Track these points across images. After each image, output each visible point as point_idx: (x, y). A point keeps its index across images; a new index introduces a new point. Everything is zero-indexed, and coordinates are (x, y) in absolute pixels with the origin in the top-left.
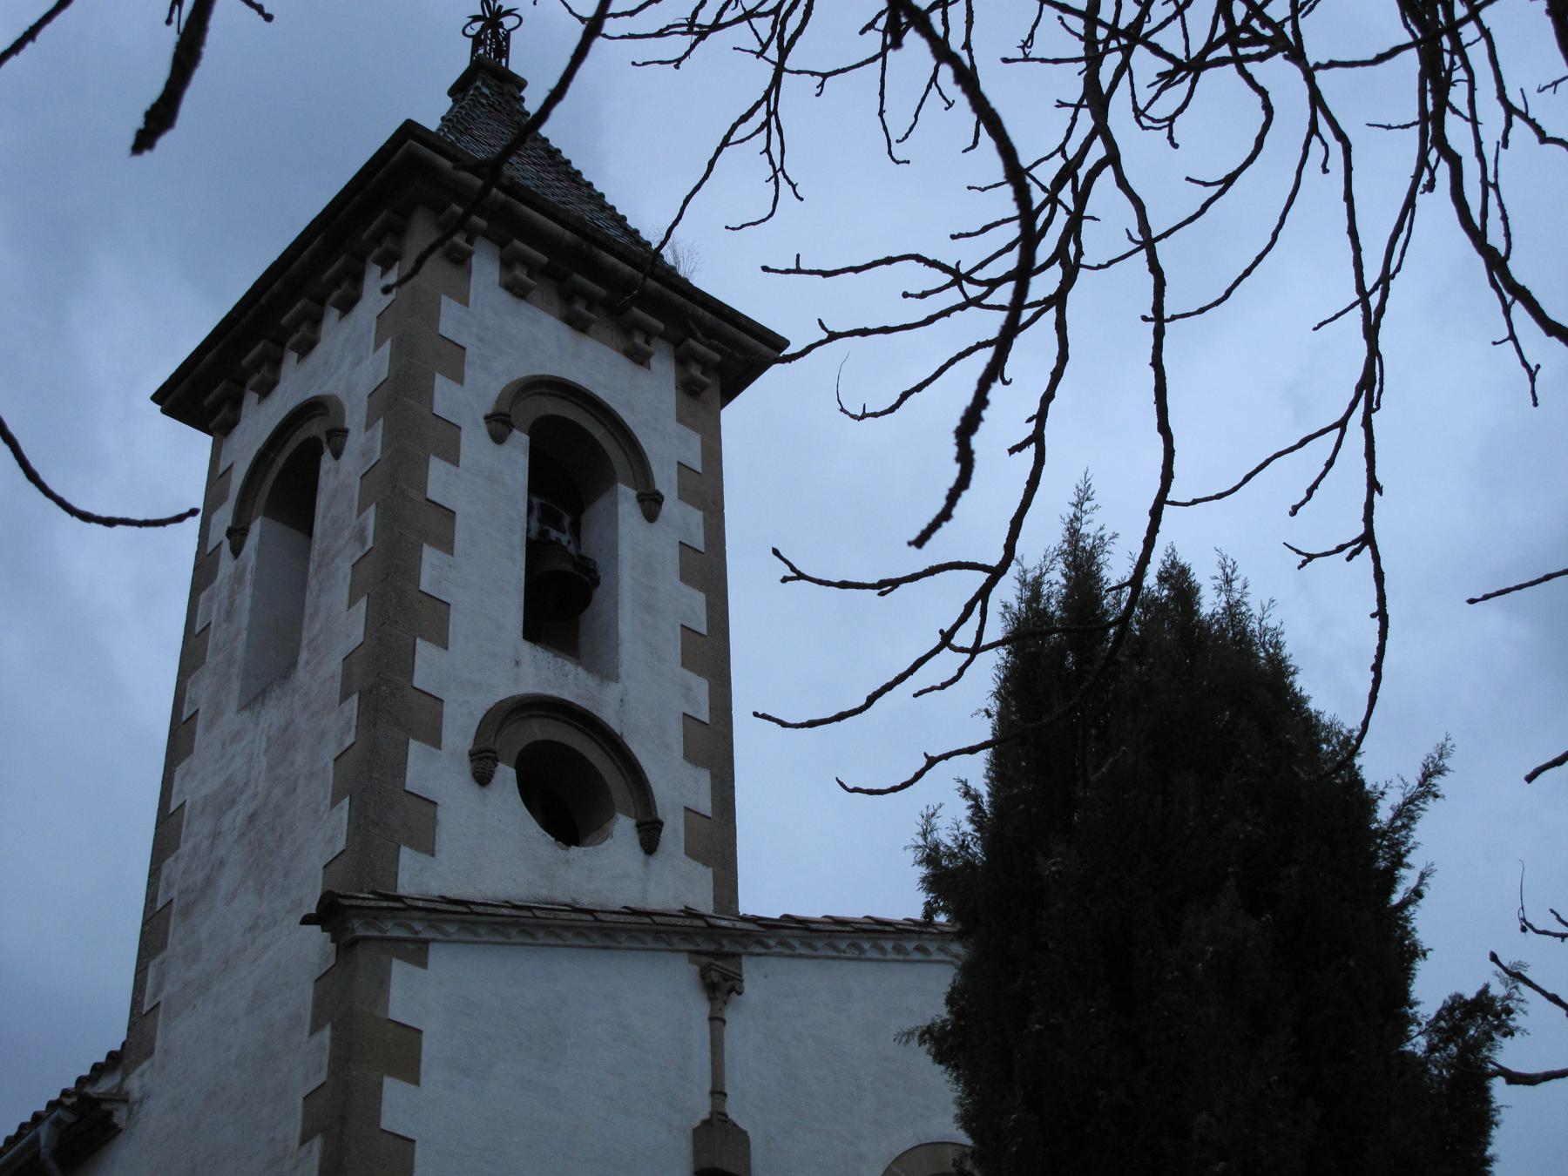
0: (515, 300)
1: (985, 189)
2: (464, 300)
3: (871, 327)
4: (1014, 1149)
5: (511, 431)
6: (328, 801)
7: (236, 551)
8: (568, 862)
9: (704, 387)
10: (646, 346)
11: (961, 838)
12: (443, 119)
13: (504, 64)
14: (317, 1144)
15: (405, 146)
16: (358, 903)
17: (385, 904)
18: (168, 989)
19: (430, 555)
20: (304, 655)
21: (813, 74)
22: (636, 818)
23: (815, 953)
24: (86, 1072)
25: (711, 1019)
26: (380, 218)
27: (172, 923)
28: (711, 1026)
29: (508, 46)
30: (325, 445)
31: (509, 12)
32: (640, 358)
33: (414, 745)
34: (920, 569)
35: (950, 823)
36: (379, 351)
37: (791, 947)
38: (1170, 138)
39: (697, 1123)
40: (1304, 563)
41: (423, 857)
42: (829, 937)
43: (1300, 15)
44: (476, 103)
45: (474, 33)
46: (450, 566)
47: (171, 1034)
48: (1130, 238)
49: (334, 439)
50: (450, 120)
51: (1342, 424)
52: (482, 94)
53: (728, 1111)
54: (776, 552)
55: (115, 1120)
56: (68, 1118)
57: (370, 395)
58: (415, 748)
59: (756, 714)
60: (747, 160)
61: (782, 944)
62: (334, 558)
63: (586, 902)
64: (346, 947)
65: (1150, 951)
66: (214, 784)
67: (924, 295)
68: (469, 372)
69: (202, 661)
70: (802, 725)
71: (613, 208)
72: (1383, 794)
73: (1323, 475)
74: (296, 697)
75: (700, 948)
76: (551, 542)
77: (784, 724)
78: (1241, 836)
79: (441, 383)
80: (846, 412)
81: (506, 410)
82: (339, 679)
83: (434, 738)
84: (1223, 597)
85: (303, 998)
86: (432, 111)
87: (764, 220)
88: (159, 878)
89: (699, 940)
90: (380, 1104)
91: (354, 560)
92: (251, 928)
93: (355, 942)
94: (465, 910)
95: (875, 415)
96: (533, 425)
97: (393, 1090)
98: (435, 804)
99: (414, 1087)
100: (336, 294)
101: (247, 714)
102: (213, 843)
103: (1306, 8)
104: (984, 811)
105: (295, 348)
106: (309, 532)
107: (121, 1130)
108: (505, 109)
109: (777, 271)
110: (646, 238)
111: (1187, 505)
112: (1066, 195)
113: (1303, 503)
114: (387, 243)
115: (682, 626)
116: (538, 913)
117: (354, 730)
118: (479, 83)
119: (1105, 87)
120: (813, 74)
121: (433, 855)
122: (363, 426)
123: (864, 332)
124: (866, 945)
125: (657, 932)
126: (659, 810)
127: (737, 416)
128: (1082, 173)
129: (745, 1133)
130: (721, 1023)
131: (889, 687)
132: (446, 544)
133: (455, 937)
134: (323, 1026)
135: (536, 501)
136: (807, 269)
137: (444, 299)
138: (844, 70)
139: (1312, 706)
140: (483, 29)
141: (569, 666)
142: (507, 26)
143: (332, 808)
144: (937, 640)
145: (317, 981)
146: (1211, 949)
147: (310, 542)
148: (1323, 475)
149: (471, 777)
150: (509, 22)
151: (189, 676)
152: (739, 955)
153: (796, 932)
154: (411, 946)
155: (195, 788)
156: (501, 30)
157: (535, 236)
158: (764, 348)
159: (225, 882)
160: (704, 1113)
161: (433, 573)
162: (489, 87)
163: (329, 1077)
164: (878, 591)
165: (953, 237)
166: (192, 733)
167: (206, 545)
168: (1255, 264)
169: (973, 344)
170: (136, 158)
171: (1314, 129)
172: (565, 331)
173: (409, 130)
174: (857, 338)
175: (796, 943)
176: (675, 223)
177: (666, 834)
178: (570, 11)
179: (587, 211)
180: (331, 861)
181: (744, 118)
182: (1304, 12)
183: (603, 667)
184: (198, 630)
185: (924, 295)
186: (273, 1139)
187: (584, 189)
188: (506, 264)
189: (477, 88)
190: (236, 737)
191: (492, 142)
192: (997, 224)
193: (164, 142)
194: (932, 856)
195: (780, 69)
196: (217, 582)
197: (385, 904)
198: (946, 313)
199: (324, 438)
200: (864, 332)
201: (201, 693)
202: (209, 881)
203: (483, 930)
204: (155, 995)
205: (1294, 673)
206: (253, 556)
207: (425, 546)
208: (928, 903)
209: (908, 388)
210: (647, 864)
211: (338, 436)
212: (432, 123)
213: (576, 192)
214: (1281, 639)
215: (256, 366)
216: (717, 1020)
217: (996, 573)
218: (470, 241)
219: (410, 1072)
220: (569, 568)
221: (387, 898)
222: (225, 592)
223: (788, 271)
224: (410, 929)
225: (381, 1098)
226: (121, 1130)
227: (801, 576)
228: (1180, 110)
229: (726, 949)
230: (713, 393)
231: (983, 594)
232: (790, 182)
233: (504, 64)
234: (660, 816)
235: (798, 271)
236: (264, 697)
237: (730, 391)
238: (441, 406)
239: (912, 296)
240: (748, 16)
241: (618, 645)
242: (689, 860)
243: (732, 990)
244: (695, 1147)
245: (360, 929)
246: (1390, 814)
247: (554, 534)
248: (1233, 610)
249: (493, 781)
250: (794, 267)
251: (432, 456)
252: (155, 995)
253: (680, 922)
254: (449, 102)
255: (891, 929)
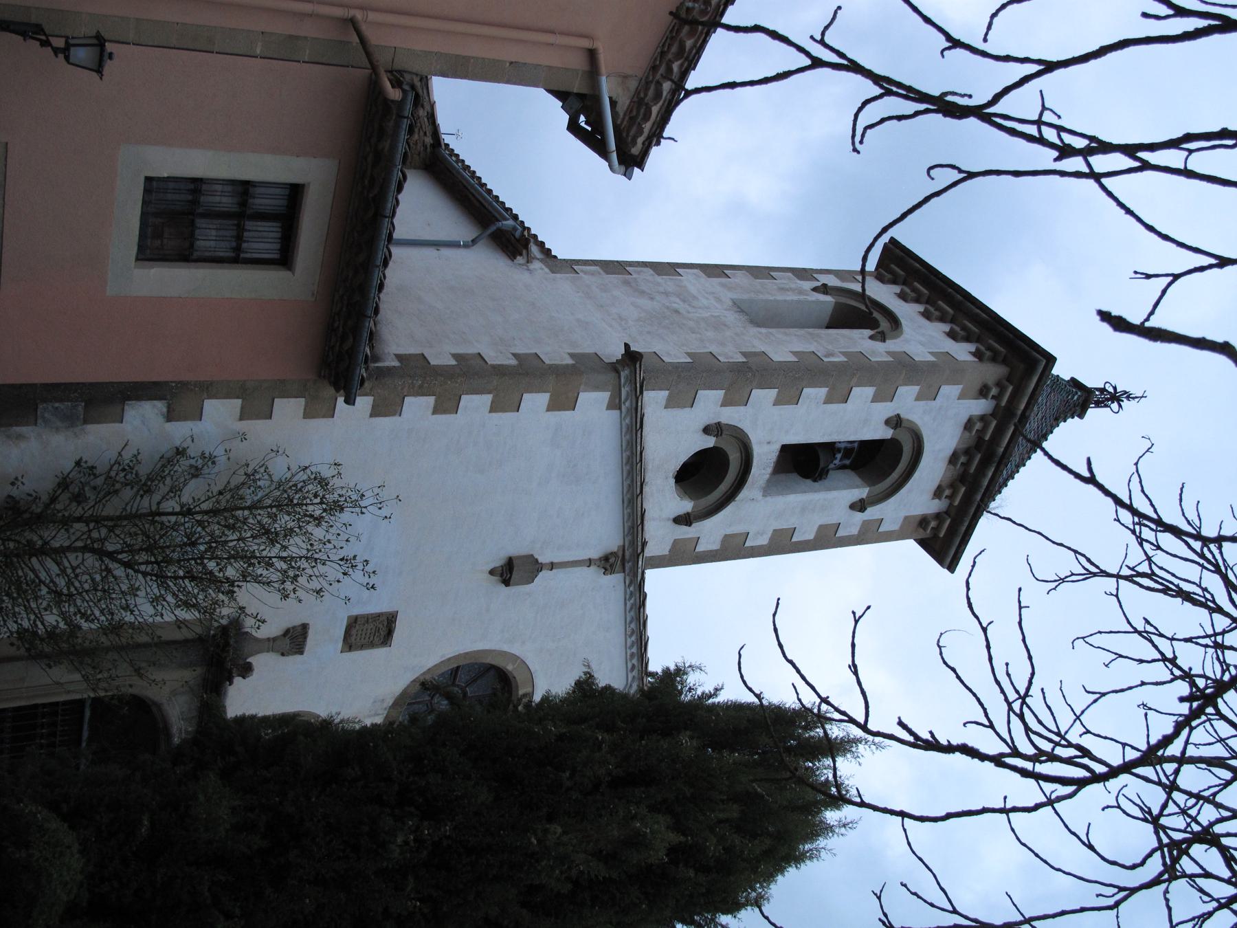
0: (963, 425)
1: (1061, 690)
2: (962, 396)
3: (991, 650)
4: (536, 730)
5: (892, 428)
6: (689, 351)
7: (815, 289)
8: (667, 478)
9: (925, 529)
10: (944, 496)
11: (694, 687)
12: (1058, 376)
13: (1091, 406)
14: (514, 362)
15: (1041, 358)
16: (638, 372)
17: (638, 385)
18: (586, 277)
19: (822, 392)
20: (763, 330)
21: (1117, 589)
22: (692, 512)
23: (627, 611)
24: (540, 239)
25: (590, 560)
26: (999, 347)
27: (620, 276)
28: (586, 560)
29: (1101, 407)
30: (876, 331)
31: (1120, 406)
32: (938, 493)
33: (721, 393)
34: (864, 686)
35: (702, 681)
36: (930, 355)
37: (630, 599)
38: (1108, 807)
39: (536, 557)
40: (876, 894)
41: (664, 403)
42: (637, 619)
43: (1187, 879)
44: (1069, 393)
45: (1107, 388)
46: (818, 403)
47: (563, 282)
48: (1053, 792)
49: (880, 335)
50: (1058, 380)
51: (955, 911)
52: (1074, 396)
53: (543, 572)
54: (869, 607)
55: (518, 257)
56: (518, 234)
57: (905, 352)
58: (720, 394)
59: (779, 599)
60: (1069, 564)
61: (631, 593)
62: (816, 341)
63: (646, 489)
64: (615, 367)
65: (644, 796)
66: (693, 290)
67: (1008, 675)
68: (922, 403)
69: (756, 277)
70: (774, 625)
71: (1018, 472)
72: (735, 917)
73: (925, 901)
74: (742, 329)
75: (626, 551)
76: (834, 455)
77: (774, 615)
78: (708, 844)
79: (915, 389)
80: (940, 636)
81: (903, 425)
82: (753, 350)
83: (726, 403)
84: (836, 823)
85: (587, 348)
86: (1062, 370)
87: (1034, 575)
88: (642, 267)
89: (630, 550)
90: (536, 392)
91: (816, 352)
92: (620, 317)
93: (617, 372)
94: (638, 427)
95: (941, 653)
96: (897, 440)
97: (543, 399)
98: (692, 407)
99: (546, 408)
100: (957, 328)
101: (731, 303)
102: (662, 293)
103: (1192, 883)
104: (709, 699)
105: (926, 310)
106: (829, 326)
107: (513, 261)
108: (1067, 409)
109: (1019, 596)
110: (1003, 491)
111: (903, 826)
112: (1072, 752)
113: (908, 890)
114: (988, 353)
115: (795, 528)
116: (639, 465)
117: (727, 361)
118: (1079, 393)
119: (1134, 771)
120: (1117, 589)
121: (665, 408)
122: (888, 350)
123: (988, 647)
124: (633, 638)
125: (633, 528)
126: (697, 523)
127: (910, 548)
128: (1086, 761)
129: (533, 582)
130: (588, 564)
131: (798, 671)
132: (829, 400)
133: (624, 423)
134: (573, 360)
135: (856, 445)
136: (1022, 613)
137: (961, 386)
138: (1121, 606)
139: (780, 878)
140: (1110, 393)
141: (770, 470)
142: (1112, 406)
143: (686, 353)
144: (824, 695)
145: (596, 354)
146: (648, 831)
147: (822, 328)
148: (925, 901)
149: (708, 424)
150: (1115, 406)
151: (747, 272)
152: (624, 572)
153: (638, 600)
154: (617, 401)
155: (690, 281)
156: (1110, 402)
157: (999, 431)
158: (949, 560)
159: (643, 302)
160: (541, 560)
161: (814, 394)
162: (1078, 399)
163: (548, 365)
164: (851, 664)
165: (1042, 690)
166: (718, 276)
167: (817, 273)
168: (1042, 859)
169: (985, 706)
170: (1095, 312)
171: (1121, 889)
172: (949, 452)
173: (1051, 360)
174: (985, 643)
175: (632, 601)
176: (1026, 528)
177: (684, 528)
178: (1141, 457)
179: (1015, 458)
180: (658, 356)
181: (1089, 560)
182: (1190, 881)
183: (770, 488)
184: (772, 273)
185: (1008, 675)
186: (514, 339)
187: (1027, 455)
188: (982, 418)
189: (1077, 393)
190: (719, 300)
191: (1048, 404)
192: (1052, 714)
193: (1106, 328)
194: (680, 672)
195: (1118, 576)
196: (799, 282)
197: (638, 385)
198: (1002, 691)
199: (879, 330)
200: (988, 647)
201: (740, 279)
202: (642, 293)
203: (628, 437)
204: (582, 271)
205: (796, 867)
206: (813, 299)
207: (826, 389)
208: (657, 673)
209: (958, 671)
210: (669, 519)
211: (882, 337)
212: (1055, 371)
213: (1025, 451)
214: (815, 860)
215: (914, 290)
216: (590, 562)
217: (864, 727)
218: (993, 397)
219: (553, 407)
220: (822, 465)
221: (641, 387)
222: (793, 286)
223: (1019, 602)
224: (626, 400)
225: (539, 392)
226: (513, 261)
227: (856, 622)
228: (1124, 812)
229: (626, 565)
230: (922, 534)
231: (852, 720)
232: (1056, 587)
233: (1091, 406)
234: (694, 525)
235: (1020, 608)
236: (739, 312)
237: (923, 543)
238: (902, 390)
239: (1007, 668)
240: (1149, 559)
241: (782, 495)
242: (672, 541)
243: (606, 569)
244: (524, 556)
245: (625, 373)
246: (724, 923)
247: (839, 456)
248: (830, 828)
249: (706, 436)
250: (1022, 605)
251: (875, 388)
252: (582, 271)
253: (639, 539)
254: (1067, 378)
255: (643, 651)
